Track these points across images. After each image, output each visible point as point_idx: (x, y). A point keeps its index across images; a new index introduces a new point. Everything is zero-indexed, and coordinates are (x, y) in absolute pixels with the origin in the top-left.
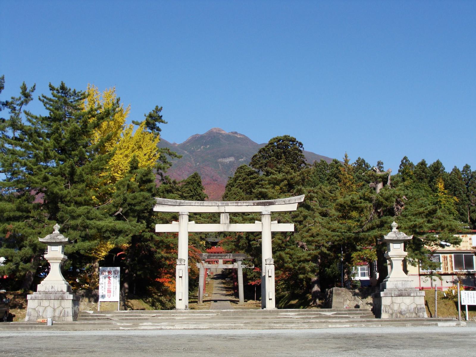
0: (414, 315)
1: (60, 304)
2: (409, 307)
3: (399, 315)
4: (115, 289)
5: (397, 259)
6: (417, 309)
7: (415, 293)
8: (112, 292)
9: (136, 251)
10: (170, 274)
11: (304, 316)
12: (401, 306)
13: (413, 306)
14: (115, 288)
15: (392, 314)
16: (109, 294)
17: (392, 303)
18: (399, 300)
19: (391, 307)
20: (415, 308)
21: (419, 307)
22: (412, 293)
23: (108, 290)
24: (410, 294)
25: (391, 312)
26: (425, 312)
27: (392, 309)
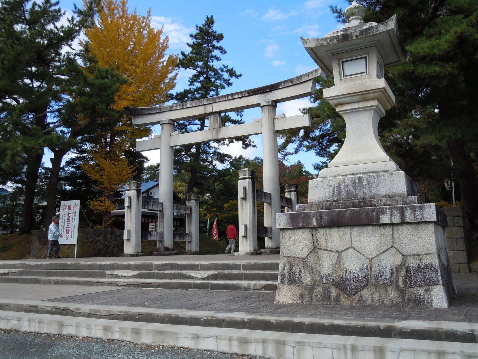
0: (392, 294)
1: (339, 261)
2: (376, 262)
3: (334, 293)
4: (73, 228)
5: (356, 106)
6: (403, 272)
7: (397, 214)
8: (70, 232)
9: (108, 149)
10: (325, 137)
11: (113, 280)
12: (344, 259)
13: (390, 261)
14: (73, 227)
15: (311, 289)
16: (67, 235)
17: (315, 248)
18: (335, 238)
19: (310, 263)
20: (398, 268)
21: (412, 263)
22: (383, 212)
23: (67, 230)
24: (378, 219)
25: (307, 279)
26: (436, 283)
27: (311, 272)
